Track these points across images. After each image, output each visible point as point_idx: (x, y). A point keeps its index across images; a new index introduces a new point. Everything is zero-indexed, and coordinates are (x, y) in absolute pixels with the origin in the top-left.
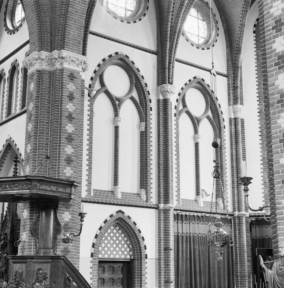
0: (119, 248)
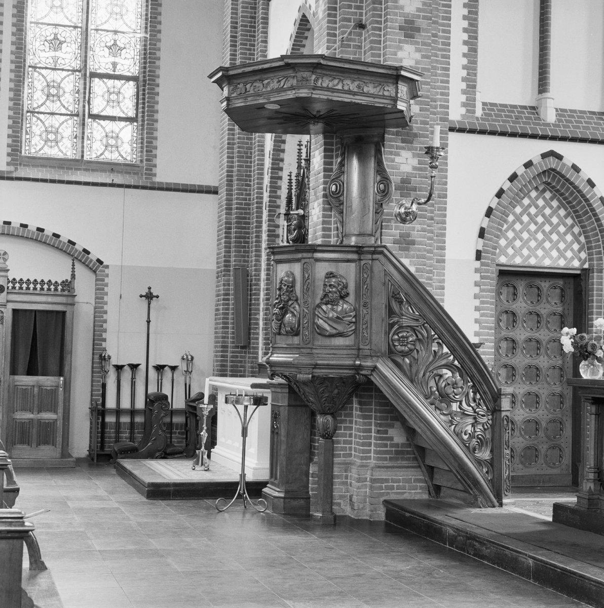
0: (551, 241)
